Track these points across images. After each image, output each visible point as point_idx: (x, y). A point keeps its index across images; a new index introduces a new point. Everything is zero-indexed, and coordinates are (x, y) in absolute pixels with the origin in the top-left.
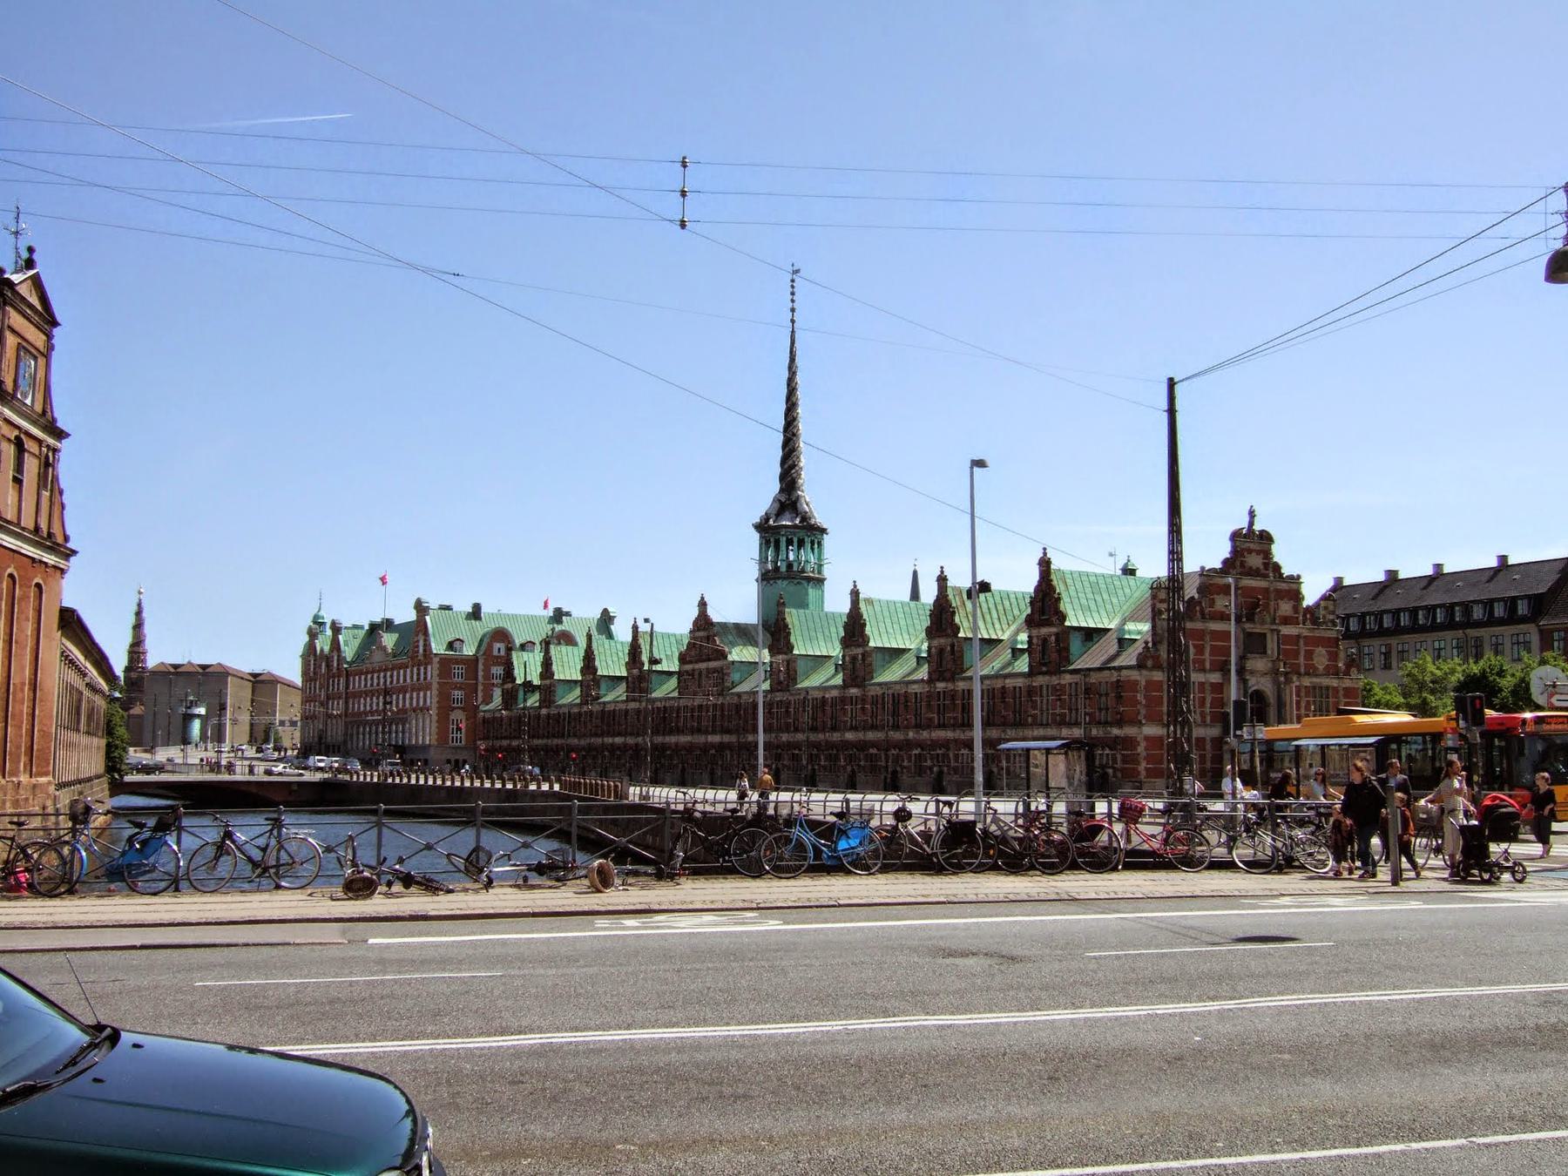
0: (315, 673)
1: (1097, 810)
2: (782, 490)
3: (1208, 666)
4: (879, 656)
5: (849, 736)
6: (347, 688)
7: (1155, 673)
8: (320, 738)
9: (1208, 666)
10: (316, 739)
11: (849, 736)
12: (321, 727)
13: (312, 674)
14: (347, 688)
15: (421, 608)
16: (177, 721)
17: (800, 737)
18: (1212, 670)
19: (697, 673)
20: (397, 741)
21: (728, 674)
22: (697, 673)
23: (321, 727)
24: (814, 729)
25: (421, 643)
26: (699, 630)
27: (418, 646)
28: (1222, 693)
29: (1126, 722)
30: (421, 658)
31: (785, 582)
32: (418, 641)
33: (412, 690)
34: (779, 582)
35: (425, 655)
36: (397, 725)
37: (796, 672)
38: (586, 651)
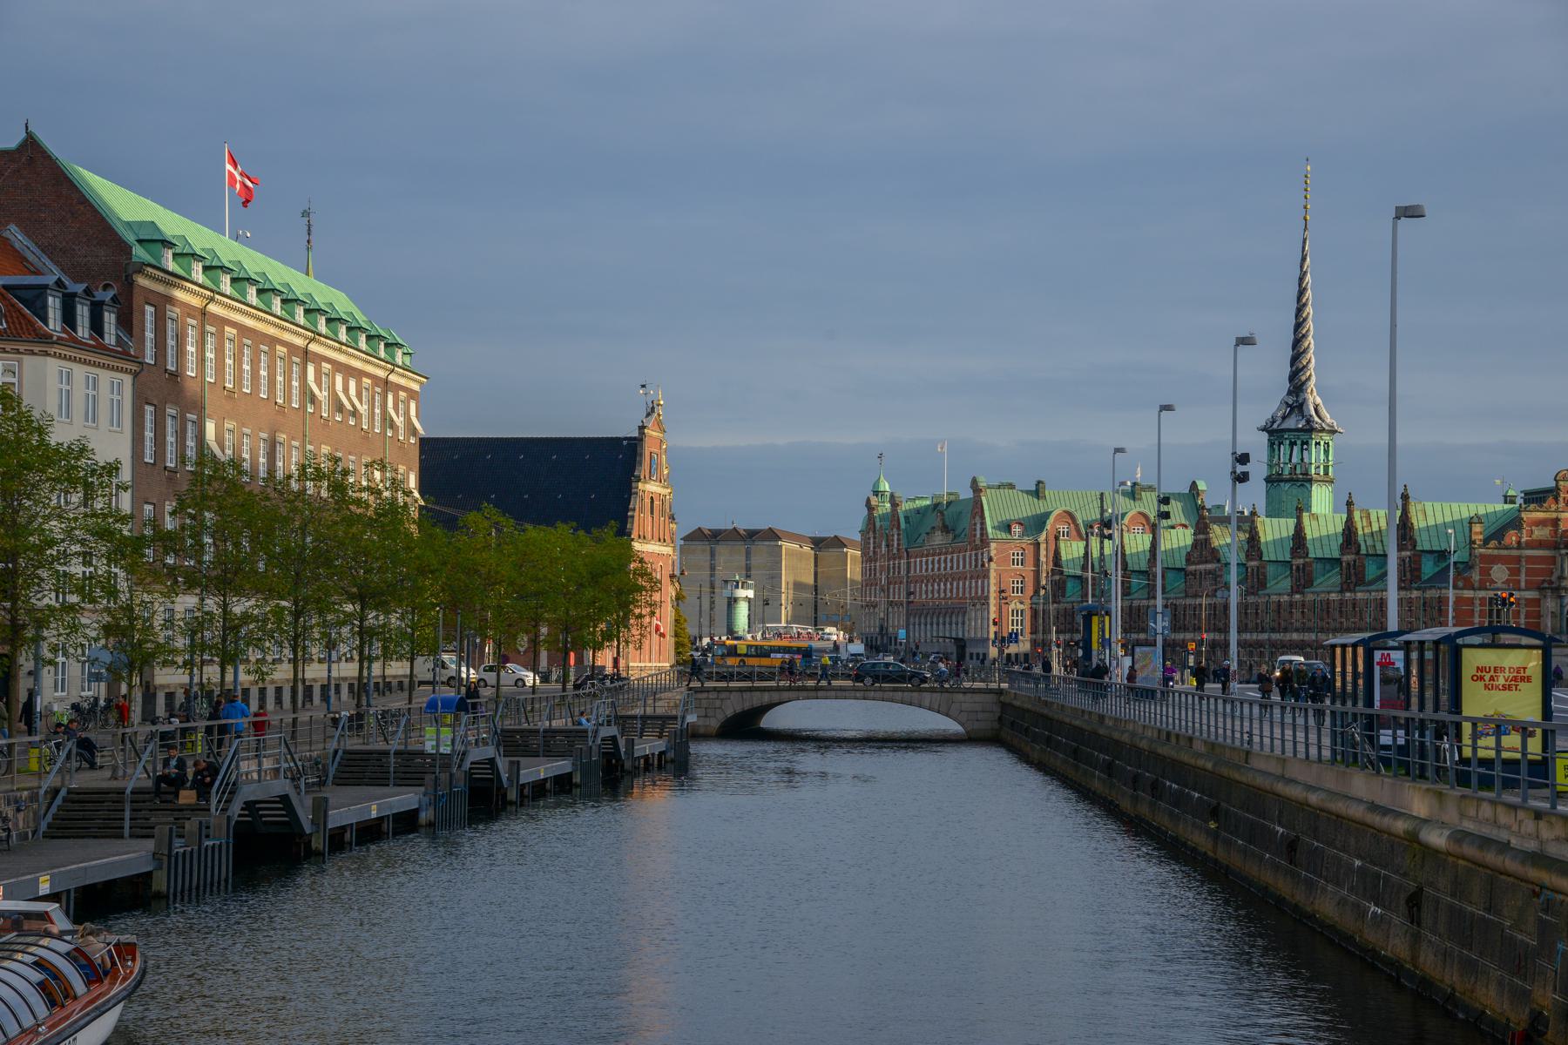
0: (874, 552)
1: (1478, 702)
2: (1290, 393)
3: (1523, 584)
4: (1320, 566)
5: (1295, 636)
6: (908, 572)
7: (1465, 592)
8: (882, 628)
9: (1523, 584)
10: (877, 630)
11: (1295, 636)
12: (882, 615)
13: (871, 554)
14: (908, 572)
15: (976, 488)
16: (721, 605)
17: (1265, 636)
18: (1527, 589)
19: (1198, 573)
20: (957, 634)
21: (1221, 576)
22: (1198, 573)
23: (882, 615)
24: (1273, 630)
25: (978, 526)
26: (1199, 533)
27: (975, 530)
28: (1539, 607)
29: (635, 772)
30: (978, 542)
31: (1288, 485)
32: (975, 524)
33: (971, 578)
34: (1282, 484)
35: (982, 541)
36: (915, 617)
37: (1265, 577)
38: (1296, 527)
